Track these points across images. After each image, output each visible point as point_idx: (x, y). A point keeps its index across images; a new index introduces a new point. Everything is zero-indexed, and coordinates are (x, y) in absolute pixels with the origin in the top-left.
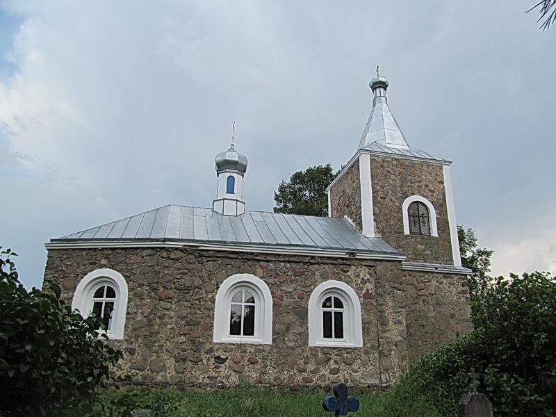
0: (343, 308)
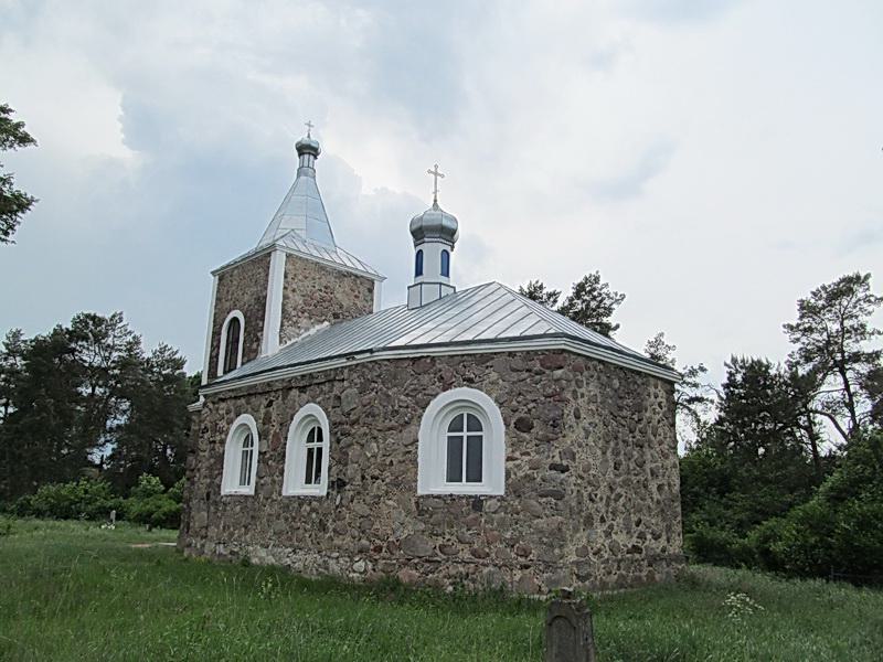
0: (481, 430)
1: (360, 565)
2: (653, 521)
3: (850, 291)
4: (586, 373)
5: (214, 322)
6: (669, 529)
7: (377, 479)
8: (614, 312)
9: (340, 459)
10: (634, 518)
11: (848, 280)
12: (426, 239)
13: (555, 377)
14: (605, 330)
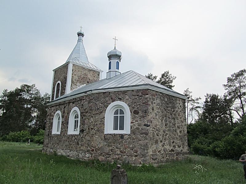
0: (124, 114)
1: (87, 155)
2: (178, 142)
3: (242, 74)
4: (156, 96)
5: (53, 84)
6: (183, 144)
7: (93, 129)
8: (173, 82)
9: (83, 123)
10: (172, 141)
11: (242, 71)
12: (112, 58)
13: (146, 97)
14: (171, 87)
